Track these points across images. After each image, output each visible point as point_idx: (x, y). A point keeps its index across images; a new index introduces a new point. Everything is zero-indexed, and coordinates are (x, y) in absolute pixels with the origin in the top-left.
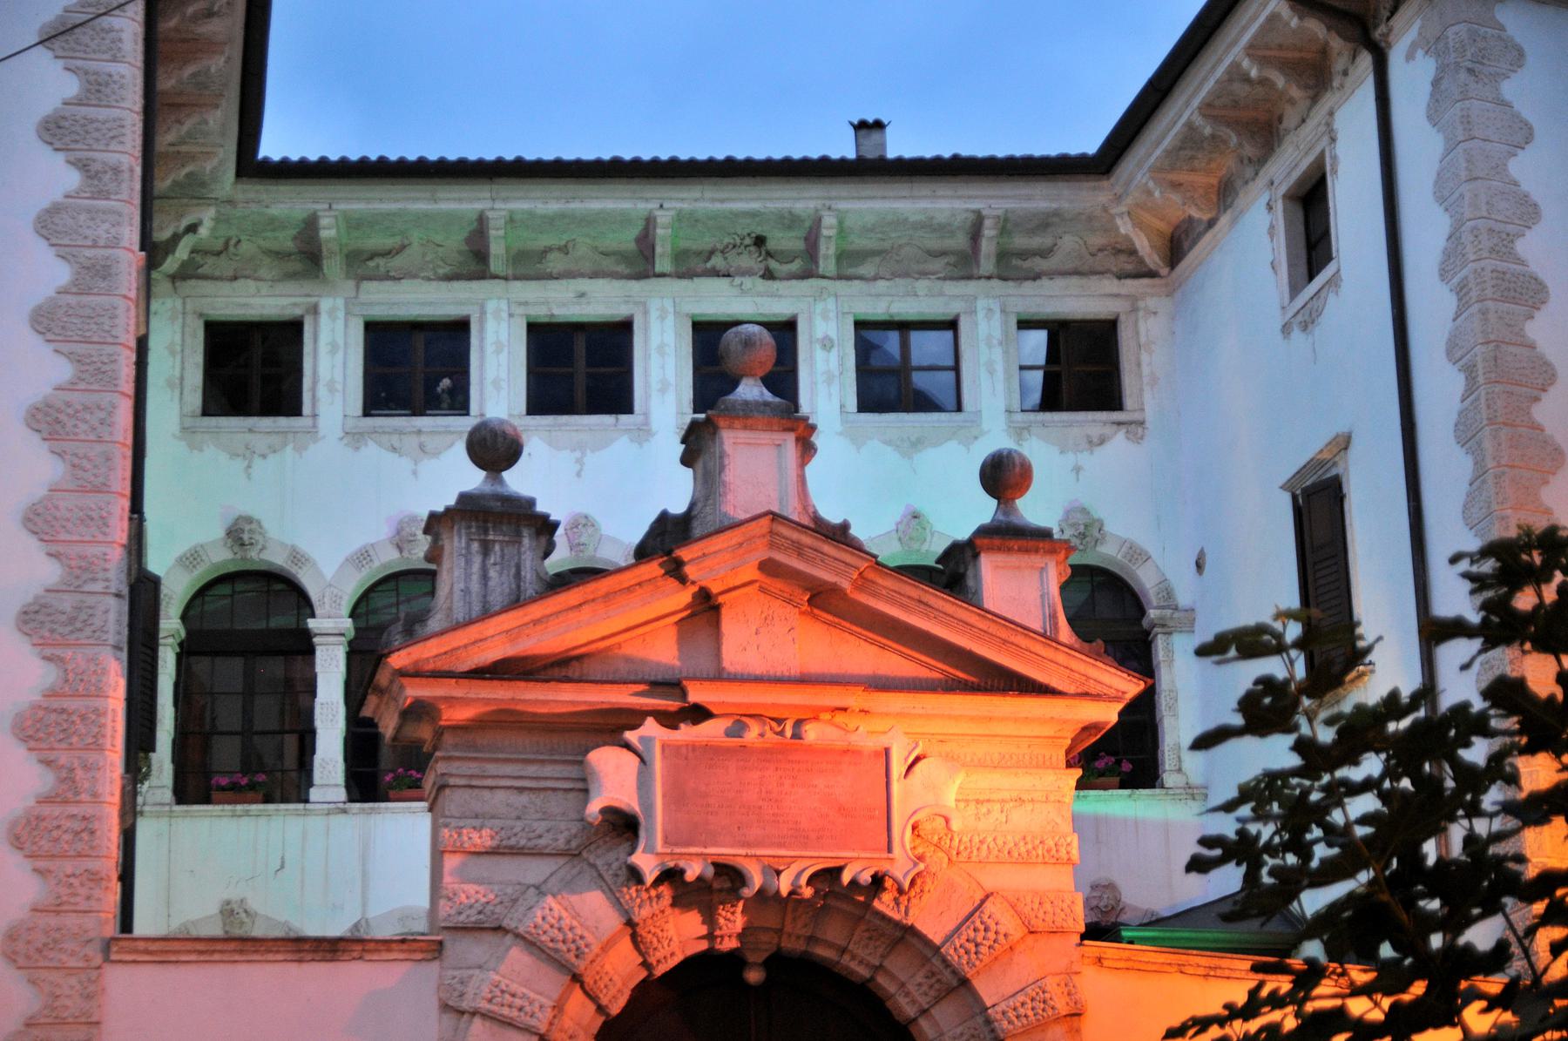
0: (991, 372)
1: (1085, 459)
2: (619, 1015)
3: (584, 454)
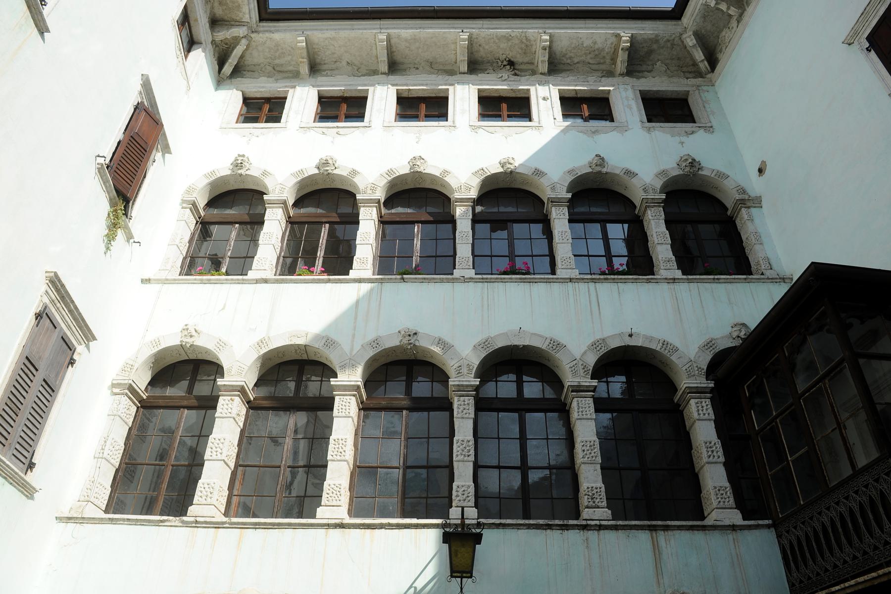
0: (631, 108)
1: (684, 139)
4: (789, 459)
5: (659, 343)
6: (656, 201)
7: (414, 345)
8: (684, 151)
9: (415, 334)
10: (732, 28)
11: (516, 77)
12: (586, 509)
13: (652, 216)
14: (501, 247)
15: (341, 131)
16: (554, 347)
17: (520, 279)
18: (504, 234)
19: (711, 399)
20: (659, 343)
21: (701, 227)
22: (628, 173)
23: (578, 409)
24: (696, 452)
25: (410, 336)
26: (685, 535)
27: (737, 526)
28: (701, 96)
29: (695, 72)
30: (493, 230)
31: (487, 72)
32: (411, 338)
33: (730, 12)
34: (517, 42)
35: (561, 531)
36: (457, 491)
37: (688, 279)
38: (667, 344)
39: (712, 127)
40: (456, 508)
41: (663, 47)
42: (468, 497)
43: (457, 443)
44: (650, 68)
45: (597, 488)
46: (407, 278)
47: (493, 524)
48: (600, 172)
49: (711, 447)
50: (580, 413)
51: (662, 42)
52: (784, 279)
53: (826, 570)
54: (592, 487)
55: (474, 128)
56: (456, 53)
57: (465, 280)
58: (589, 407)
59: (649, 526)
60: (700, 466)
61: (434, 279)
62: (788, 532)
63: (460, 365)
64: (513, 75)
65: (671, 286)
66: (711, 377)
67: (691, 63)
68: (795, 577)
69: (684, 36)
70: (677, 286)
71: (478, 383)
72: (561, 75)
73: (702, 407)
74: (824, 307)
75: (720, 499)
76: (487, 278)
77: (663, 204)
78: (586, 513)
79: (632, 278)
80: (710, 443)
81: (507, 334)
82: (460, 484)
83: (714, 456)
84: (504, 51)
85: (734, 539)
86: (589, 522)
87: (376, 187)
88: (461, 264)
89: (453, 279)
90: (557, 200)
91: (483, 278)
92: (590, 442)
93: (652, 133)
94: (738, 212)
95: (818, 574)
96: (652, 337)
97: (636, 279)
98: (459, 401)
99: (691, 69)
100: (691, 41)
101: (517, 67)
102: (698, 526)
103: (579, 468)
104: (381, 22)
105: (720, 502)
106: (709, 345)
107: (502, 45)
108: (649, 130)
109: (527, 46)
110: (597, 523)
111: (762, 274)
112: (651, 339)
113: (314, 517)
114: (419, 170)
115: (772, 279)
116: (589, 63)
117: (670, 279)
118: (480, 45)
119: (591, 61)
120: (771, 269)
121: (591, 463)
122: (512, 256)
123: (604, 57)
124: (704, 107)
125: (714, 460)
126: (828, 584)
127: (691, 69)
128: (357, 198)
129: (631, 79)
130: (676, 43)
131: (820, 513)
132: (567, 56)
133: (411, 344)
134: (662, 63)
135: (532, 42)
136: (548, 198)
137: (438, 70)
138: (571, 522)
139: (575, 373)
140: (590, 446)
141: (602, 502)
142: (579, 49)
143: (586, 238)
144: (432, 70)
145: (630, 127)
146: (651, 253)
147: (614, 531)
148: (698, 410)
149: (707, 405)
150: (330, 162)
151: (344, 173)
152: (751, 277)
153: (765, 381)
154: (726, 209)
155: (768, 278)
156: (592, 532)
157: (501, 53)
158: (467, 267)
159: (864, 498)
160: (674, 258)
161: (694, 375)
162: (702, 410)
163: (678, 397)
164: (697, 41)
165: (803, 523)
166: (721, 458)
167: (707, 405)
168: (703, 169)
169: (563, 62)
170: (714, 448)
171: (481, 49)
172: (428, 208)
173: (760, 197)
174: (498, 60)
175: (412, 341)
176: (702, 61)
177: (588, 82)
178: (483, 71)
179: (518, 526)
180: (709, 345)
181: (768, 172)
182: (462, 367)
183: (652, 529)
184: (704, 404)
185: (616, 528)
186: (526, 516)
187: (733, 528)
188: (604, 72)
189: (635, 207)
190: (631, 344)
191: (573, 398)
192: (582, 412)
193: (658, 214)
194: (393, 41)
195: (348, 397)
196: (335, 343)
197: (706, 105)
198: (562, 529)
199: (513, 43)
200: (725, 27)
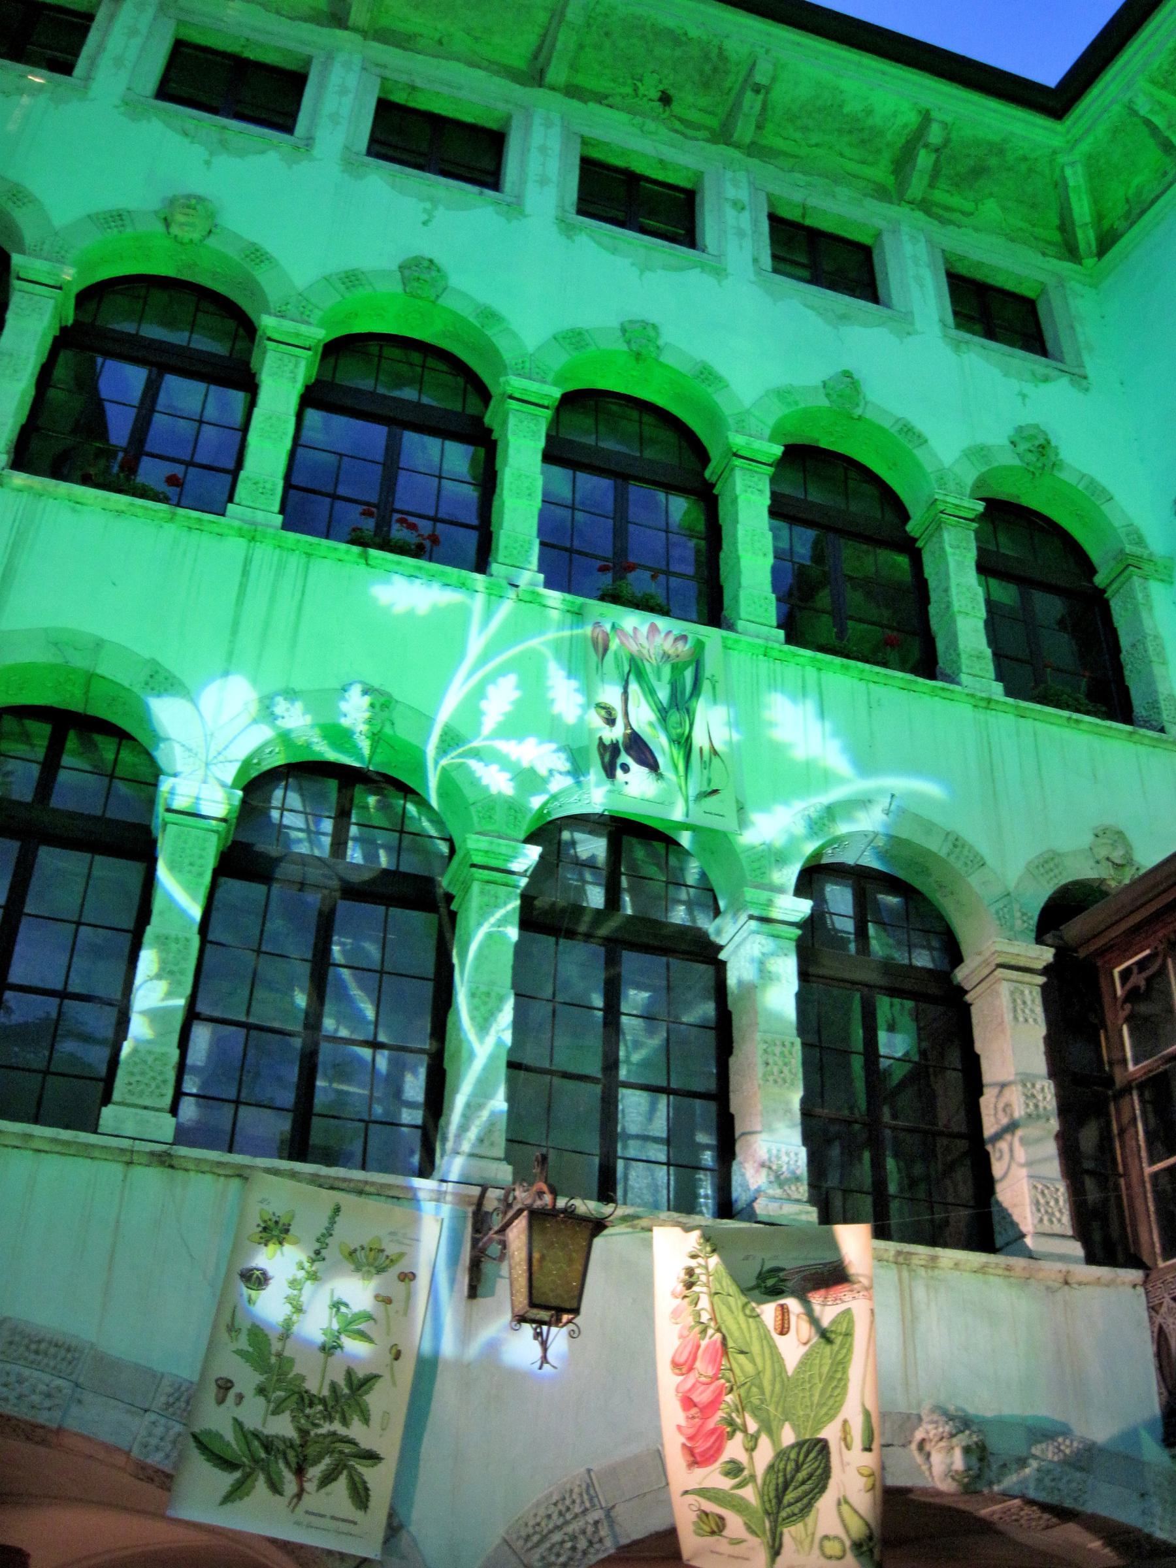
0: (922, 286)
1: (1028, 388)
2: (403, 1076)
3: (435, 207)
8: (1027, 416)
38: (963, 846)
41: (1009, 169)
51: (1010, 158)
55: (349, 164)
65: (981, 715)
66: (1048, 938)
93: (965, 356)
106: (1047, 866)
108: (957, 346)
109: (715, 70)
119: (848, 152)
146: (722, 578)
152: (952, 687)
160: (988, 652)
172: (195, 336)
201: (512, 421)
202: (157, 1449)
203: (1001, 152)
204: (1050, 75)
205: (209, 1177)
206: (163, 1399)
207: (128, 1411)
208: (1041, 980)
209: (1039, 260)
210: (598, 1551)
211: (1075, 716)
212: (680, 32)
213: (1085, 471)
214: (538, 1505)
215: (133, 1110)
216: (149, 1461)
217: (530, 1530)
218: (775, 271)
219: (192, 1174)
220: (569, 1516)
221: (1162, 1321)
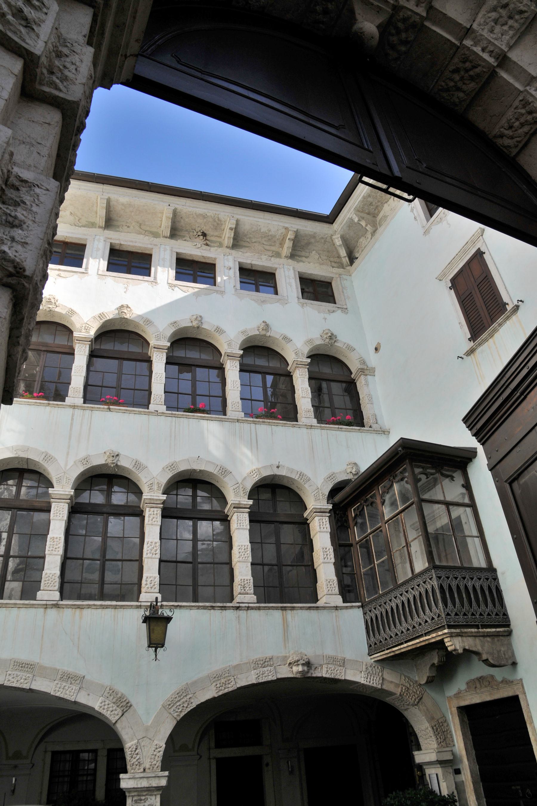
1: (327, 316)
4: (376, 563)
5: (297, 474)
6: (303, 363)
7: (117, 465)
9: (118, 455)
10: (368, 238)
11: (207, 247)
12: (239, 595)
13: (300, 375)
14: (186, 386)
15: (62, 274)
16: (223, 473)
17: (201, 417)
18: (188, 376)
19: (329, 517)
20: (297, 474)
21: (333, 384)
22: (285, 338)
23: (238, 521)
24: (316, 554)
25: (113, 457)
26: (305, 613)
27: (339, 607)
28: (341, 283)
29: (338, 263)
30: (180, 372)
31: (184, 239)
32: (114, 458)
33: (367, 228)
34: (211, 220)
35: (221, 611)
36: (146, 581)
37: (321, 427)
39: (347, 309)
40: (145, 594)
42: (154, 585)
43: (147, 544)
44: (307, 254)
45: (247, 580)
46: (113, 409)
47: (173, 606)
48: (265, 335)
49: (326, 552)
50: (239, 524)
52: (384, 431)
53: (391, 637)
54: (244, 580)
55: (171, 286)
56: (162, 220)
57: (157, 413)
58: (245, 520)
59: (282, 607)
60: (318, 565)
61: (134, 411)
62: (370, 611)
63: (151, 483)
64: (205, 245)
65: (309, 431)
66: (330, 502)
67: (337, 255)
68: (372, 640)
69: (334, 237)
70: (313, 431)
71: (165, 498)
72: (241, 250)
73: (323, 523)
74: (405, 466)
75: (329, 588)
76: (175, 414)
77: (308, 367)
78: (238, 598)
79: (282, 423)
80: (326, 549)
81: (188, 459)
82: (149, 575)
83: (328, 558)
84: (201, 225)
85: (336, 616)
86: (241, 605)
87: (90, 327)
88: (155, 400)
89: (149, 412)
90: (232, 355)
91: (172, 414)
92: (245, 546)
94: (359, 377)
95: (386, 639)
96: (293, 469)
97: (285, 424)
98: (149, 511)
99: (336, 260)
100: (338, 242)
101: (208, 238)
102: (313, 607)
103: (235, 564)
104: (104, 187)
105: (329, 590)
107: (199, 221)
108: (303, 305)
109: (218, 224)
110: (247, 605)
111: (371, 427)
112: (292, 471)
113: (35, 599)
114: (125, 317)
115: (376, 431)
116: (263, 244)
117: (309, 426)
118: (181, 218)
119: (265, 243)
120: (377, 423)
121: (244, 562)
122: (194, 395)
123: (275, 242)
124: (343, 292)
125: (327, 561)
126: (391, 646)
127: (336, 260)
128: (74, 335)
129: (293, 262)
130: (328, 241)
131: (390, 600)
132: (248, 236)
133: (114, 463)
134: (316, 252)
135: (222, 222)
136: (225, 352)
137: (146, 231)
138: (229, 604)
139: (236, 494)
140: (244, 549)
141: (250, 590)
142: (257, 233)
143: (250, 386)
144: (141, 230)
145: (289, 301)
147: (258, 611)
148: (320, 525)
149: (326, 522)
150: (53, 301)
151: (64, 312)
152: (363, 428)
153: (365, 507)
154: (351, 373)
155: (374, 431)
156: (242, 611)
157: (197, 225)
158: (160, 403)
159: (417, 593)
161: (319, 499)
162: (323, 525)
163: (307, 514)
164: (342, 242)
165: (380, 606)
166: (332, 559)
167: (326, 522)
168: (338, 341)
169: (244, 240)
170: (328, 552)
171: (182, 221)
173: (375, 368)
174: (194, 231)
175: (115, 461)
176: (345, 257)
177: (261, 259)
178: (182, 237)
179: (191, 607)
180: (331, 478)
181: (381, 350)
182: (153, 484)
183: (283, 609)
184: (324, 520)
185: (259, 608)
186: (195, 600)
187: (336, 608)
188: (274, 253)
189: (288, 365)
190: (278, 473)
191: (234, 513)
192: (240, 523)
193: (304, 373)
194: (112, 203)
195: (63, 504)
196: (53, 458)
197: (345, 291)
198: (222, 610)
199: (207, 220)
200: (362, 236)
201: (155, 355)
202: (58, 691)
203: (314, 237)
204: (327, 210)
205: (70, 609)
206: (60, 676)
207: (50, 681)
208: (328, 515)
209: (331, 269)
210: (191, 706)
211: (340, 427)
212: (204, 214)
213: (345, 342)
214: (172, 695)
215: (47, 592)
216: (56, 695)
217: (170, 703)
218: (241, 289)
219: (65, 609)
220: (182, 697)
221: (414, 593)
